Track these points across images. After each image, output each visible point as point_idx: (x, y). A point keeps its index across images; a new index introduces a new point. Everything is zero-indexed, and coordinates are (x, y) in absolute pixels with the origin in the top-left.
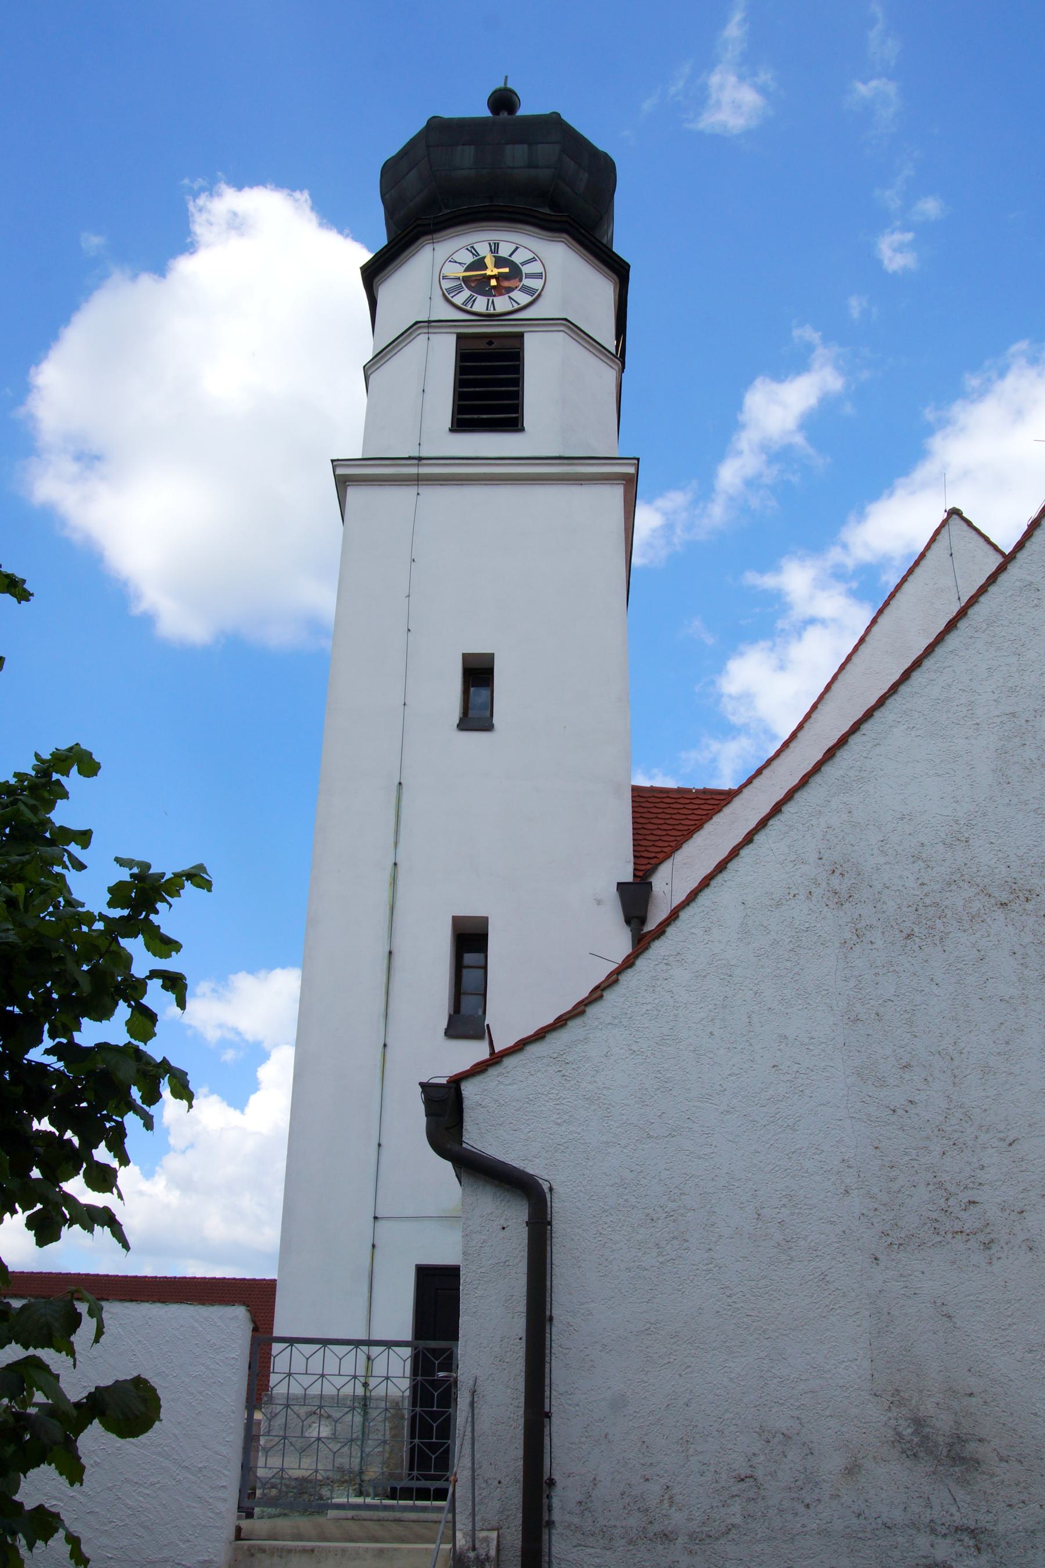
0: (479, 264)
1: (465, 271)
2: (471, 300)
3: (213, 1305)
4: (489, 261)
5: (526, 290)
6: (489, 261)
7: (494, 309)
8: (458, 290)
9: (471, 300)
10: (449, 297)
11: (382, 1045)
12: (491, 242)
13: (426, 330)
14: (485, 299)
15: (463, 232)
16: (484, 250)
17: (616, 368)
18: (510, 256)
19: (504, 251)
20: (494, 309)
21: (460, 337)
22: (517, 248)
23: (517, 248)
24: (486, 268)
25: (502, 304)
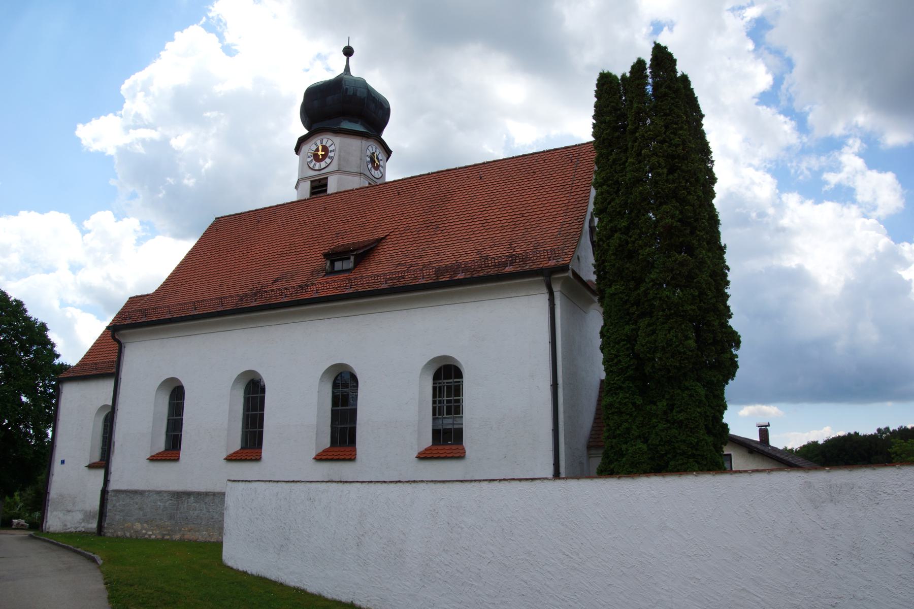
0: (317, 150)
2: (315, 165)
5: (330, 158)
6: (320, 148)
9: (315, 165)
16: (319, 143)
19: (324, 144)
25: (323, 164)
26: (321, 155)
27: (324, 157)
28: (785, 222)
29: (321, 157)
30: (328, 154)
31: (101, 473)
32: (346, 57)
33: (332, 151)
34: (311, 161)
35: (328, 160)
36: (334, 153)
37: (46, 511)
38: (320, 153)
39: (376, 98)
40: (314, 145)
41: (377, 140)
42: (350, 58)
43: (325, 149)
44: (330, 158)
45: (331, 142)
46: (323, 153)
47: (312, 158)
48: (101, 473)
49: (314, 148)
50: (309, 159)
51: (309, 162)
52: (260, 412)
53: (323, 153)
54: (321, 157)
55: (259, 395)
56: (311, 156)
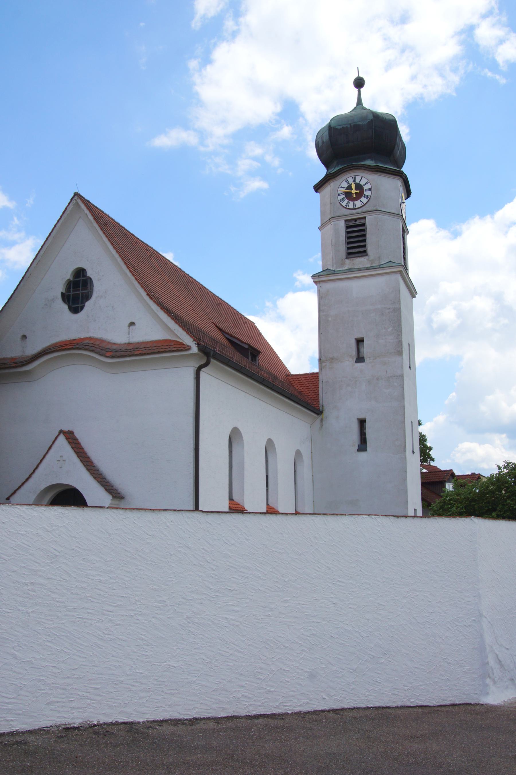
0: (349, 187)
1: (346, 190)
2: (348, 204)
3: (80, 507)
4: (353, 186)
5: (367, 197)
6: (353, 186)
7: (363, 203)
8: (342, 200)
9: (348, 204)
10: (341, 203)
11: (313, 501)
12: (346, 180)
13: (330, 223)
14: (352, 202)
15: (341, 172)
16: (351, 180)
17: (400, 218)
18: (360, 182)
19: (357, 181)
20: (363, 203)
21: (346, 221)
22: (362, 178)
23: (362, 178)
24: (352, 189)
25: (358, 204)
26: (356, 193)
27: (359, 196)
28: (498, 473)
29: (354, 196)
30: (364, 193)
31: (294, 512)
32: (357, 90)
33: (369, 190)
34: (342, 200)
35: (364, 200)
36: (370, 192)
37: (103, 345)
38: (354, 191)
39: (345, 126)
40: (344, 182)
41: (345, 171)
42: (361, 90)
43: (358, 186)
44: (367, 197)
45: (366, 181)
46: (358, 191)
47: (344, 196)
48: (294, 512)
49: (345, 185)
50: (340, 197)
51: (341, 200)
52: (81, 305)
53: (358, 191)
54: (354, 196)
55: (81, 292)
56: (341, 194)
